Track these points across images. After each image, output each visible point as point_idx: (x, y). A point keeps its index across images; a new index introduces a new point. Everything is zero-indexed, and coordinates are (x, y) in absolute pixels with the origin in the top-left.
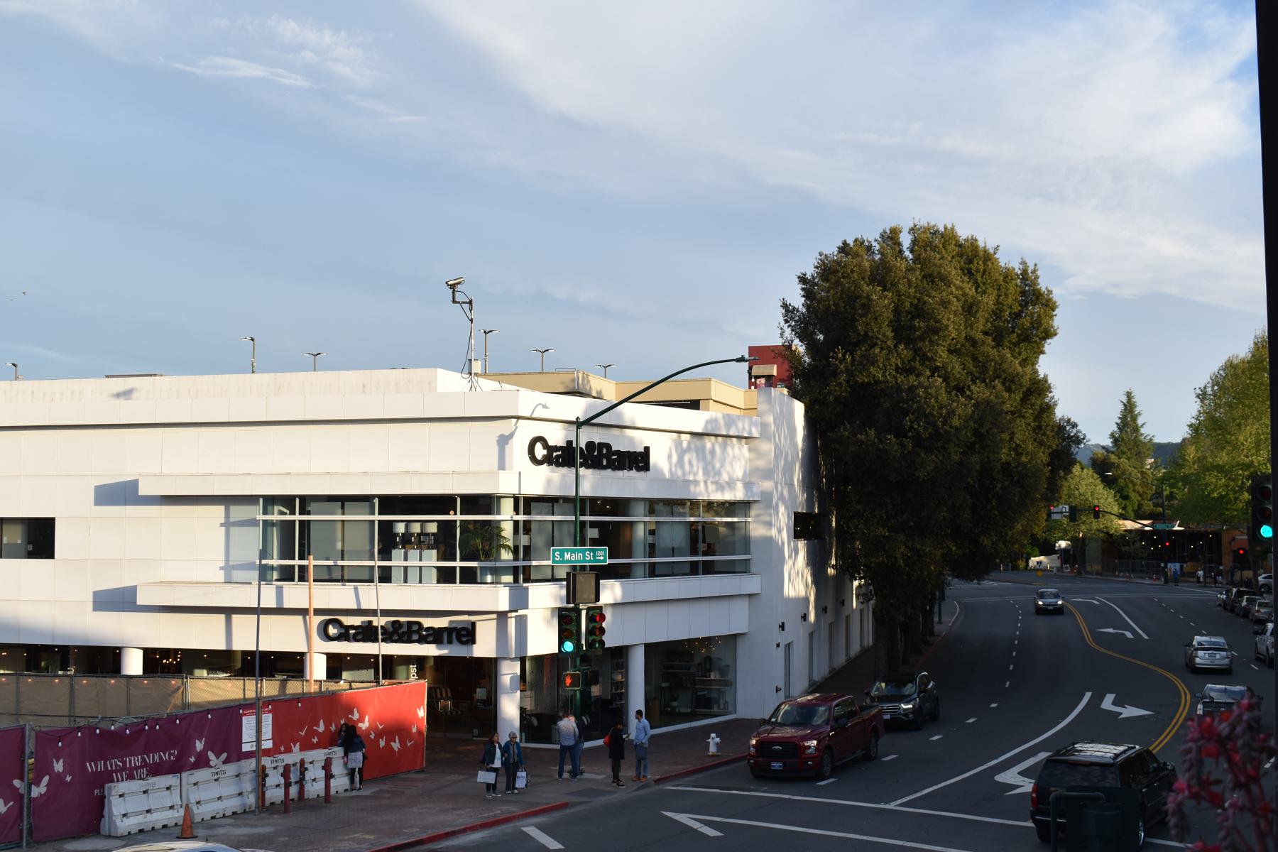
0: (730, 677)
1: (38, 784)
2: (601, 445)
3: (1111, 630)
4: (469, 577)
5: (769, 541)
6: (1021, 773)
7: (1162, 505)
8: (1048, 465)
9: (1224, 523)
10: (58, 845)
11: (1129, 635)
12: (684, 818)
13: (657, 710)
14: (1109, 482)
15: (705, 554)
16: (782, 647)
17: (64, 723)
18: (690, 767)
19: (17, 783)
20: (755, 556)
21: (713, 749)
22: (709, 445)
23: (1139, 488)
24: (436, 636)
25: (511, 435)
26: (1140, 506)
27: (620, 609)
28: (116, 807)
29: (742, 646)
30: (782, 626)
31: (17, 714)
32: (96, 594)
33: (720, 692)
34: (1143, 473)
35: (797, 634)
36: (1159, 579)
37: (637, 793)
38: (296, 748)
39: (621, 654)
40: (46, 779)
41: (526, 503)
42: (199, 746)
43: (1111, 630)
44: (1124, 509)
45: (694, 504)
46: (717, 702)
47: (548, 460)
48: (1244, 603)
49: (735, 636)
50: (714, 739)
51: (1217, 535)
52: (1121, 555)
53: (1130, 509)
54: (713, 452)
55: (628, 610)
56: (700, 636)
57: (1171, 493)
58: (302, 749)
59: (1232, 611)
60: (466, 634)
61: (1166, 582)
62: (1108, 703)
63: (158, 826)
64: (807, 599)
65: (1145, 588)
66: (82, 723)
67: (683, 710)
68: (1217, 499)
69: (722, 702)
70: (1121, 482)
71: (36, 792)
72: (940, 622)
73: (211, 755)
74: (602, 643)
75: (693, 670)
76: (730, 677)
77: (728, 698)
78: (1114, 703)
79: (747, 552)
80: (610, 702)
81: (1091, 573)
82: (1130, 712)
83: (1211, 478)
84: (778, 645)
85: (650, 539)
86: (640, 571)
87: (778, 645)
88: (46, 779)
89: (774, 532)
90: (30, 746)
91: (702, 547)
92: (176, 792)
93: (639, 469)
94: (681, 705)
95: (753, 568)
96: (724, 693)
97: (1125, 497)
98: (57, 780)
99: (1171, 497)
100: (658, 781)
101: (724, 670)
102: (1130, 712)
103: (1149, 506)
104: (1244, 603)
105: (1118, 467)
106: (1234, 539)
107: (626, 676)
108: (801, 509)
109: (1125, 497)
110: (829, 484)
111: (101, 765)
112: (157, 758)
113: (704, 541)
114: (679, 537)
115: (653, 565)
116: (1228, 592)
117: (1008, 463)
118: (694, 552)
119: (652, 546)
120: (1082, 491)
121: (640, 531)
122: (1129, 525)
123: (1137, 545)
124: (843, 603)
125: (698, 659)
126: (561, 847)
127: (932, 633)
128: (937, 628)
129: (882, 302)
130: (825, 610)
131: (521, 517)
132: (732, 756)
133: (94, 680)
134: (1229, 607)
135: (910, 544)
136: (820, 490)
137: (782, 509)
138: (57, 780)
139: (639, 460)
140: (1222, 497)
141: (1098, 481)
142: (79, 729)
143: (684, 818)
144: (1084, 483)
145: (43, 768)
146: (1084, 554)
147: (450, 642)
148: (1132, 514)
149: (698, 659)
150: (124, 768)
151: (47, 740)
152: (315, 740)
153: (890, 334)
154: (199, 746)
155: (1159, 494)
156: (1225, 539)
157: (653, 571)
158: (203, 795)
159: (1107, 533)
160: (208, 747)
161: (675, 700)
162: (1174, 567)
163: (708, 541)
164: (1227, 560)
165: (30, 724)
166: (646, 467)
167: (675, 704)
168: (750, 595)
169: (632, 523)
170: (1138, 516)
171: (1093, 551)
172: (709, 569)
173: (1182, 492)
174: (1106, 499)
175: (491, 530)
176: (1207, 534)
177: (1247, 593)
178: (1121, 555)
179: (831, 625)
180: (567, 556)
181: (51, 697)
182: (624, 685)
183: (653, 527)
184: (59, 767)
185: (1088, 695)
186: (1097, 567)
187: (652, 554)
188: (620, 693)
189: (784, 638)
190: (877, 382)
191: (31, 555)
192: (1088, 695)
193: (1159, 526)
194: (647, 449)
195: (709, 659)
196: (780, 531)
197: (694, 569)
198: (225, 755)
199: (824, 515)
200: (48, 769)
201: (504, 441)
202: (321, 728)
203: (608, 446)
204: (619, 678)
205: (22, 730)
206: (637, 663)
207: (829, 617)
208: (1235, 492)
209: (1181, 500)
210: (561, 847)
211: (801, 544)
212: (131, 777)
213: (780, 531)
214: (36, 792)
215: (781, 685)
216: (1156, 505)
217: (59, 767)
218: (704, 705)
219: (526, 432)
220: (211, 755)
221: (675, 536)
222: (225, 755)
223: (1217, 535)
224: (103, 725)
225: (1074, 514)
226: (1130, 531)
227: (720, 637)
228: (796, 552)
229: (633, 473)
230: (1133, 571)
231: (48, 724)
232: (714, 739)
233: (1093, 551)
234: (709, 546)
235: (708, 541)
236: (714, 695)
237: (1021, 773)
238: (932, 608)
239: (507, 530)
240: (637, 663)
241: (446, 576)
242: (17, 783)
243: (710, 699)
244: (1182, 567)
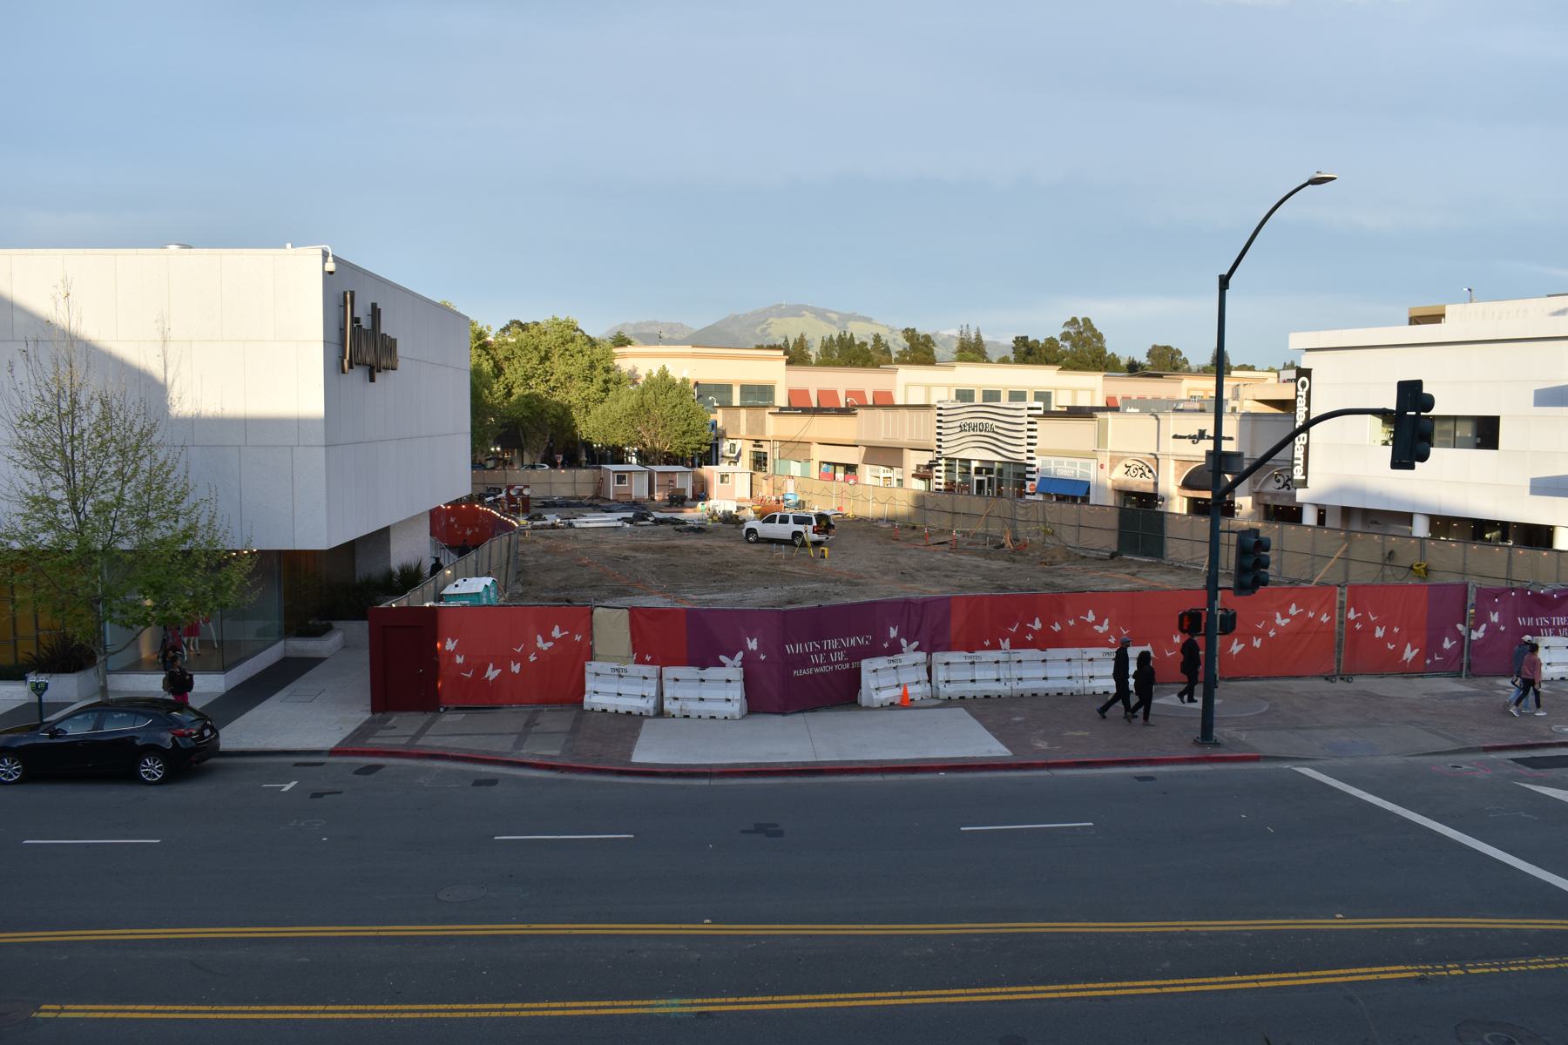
1: (1477, 630)
10: (1491, 680)
17: (1503, 584)
19: (1460, 626)
28: (868, 681)
31: (1463, 573)
32: (1533, 480)
38: (1006, 644)
40: (1484, 627)
42: (893, 633)
58: (1013, 646)
63: (1557, 677)
66: (1516, 585)
71: (1475, 635)
73: (903, 642)
88: (1484, 627)
90: (1472, 599)
92: (667, 693)
98: (1492, 628)
111: (799, 647)
112: (853, 642)
133: (1529, 551)
138: (1492, 628)
142: (1513, 590)
145: (1481, 618)
150: (1550, 626)
151: (1486, 595)
152: (1030, 638)
154: (893, 633)
158: (882, 682)
160: (900, 635)
165: (1473, 582)
181: (1491, 565)
184: (1495, 618)
185: (48, 1011)
191: (1479, 446)
198: (916, 644)
200: (1486, 619)
202: (1038, 625)
205: (1466, 586)
212: (1556, 634)
214: (1475, 635)
217: (1495, 618)
220: (903, 642)
222: (916, 644)
224: (1534, 588)
231: (1488, 583)
242: (1460, 626)
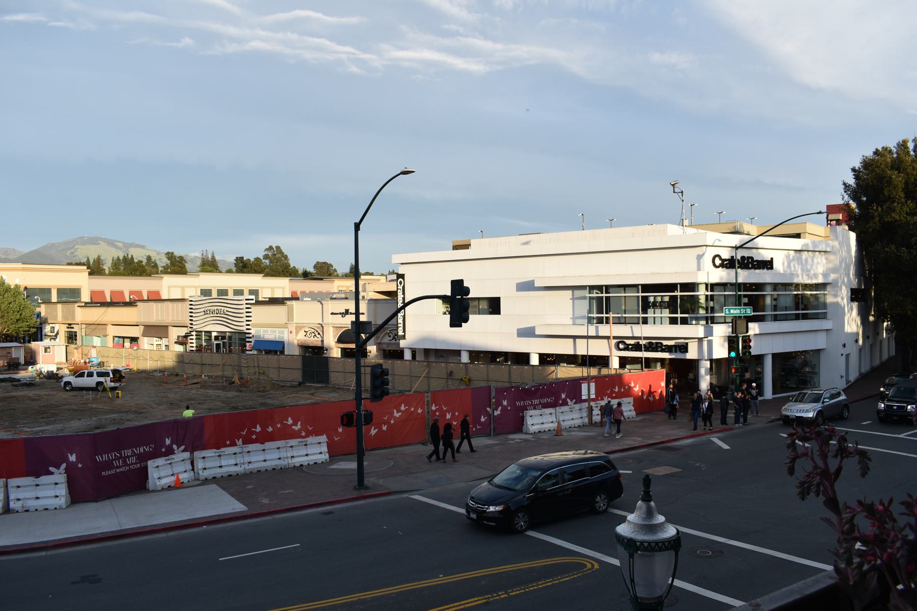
0: (816, 370)
2: (748, 258)
4: (684, 321)
5: (837, 304)
22: (804, 257)
24: (669, 349)
25: (703, 254)
29: (823, 356)
30: (844, 345)
39: (760, 358)
41: (712, 287)
47: (722, 265)
49: (819, 350)
54: (806, 260)
60: (684, 348)
64: (858, 334)
74: (750, 353)
76: (816, 370)
77: (815, 380)
85: (774, 303)
86: (769, 318)
91: (801, 306)
93: (768, 269)
95: (829, 316)
110: (870, 273)
114: (789, 302)
118: (797, 309)
121: (768, 301)
129: (898, 179)
130: (868, 337)
131: (709, 293)
136: (865, 277)
137: (844, 288)
139: (768, 265)
147: (676, 352)
153: (902, 195)
157: (776, 318)
163: (804, 303)
166: (772, 268)
168: (827, 330)
172: (805, 317)
175: (695, 299)
179: (871, 345)
180: (732, 311)
187: (775, 310)
189: (845, 351)
190: (896, 221)
194: (772, 259)
196: (842, 299)
197: (797, 317)
199: (867, 290)
201: (700, 257)
203: (752, 258)
211: (855, 305)
215: (844, 374)
219: (710, 253)
229: (765, 270)
239: (702, 300)
241: (673, 321)
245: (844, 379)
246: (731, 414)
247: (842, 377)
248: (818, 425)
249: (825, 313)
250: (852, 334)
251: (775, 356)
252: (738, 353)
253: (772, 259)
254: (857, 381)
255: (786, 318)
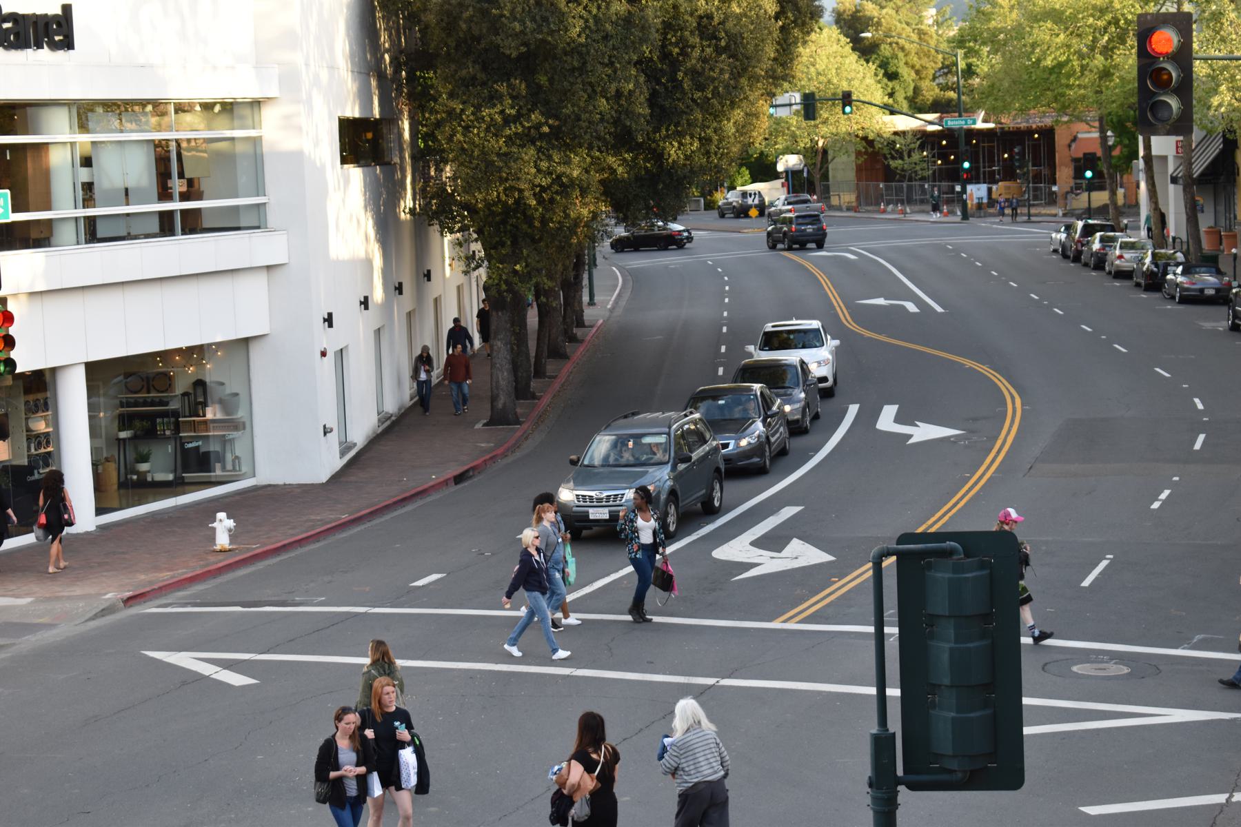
0: (241, 414)
3: (881, 301)
5: (297, 157)
6: (755, 544)
7: (955, 88)
8: (777, 17)
9: (1063, 109)
11: (911, 307)
12: (185, 660)
13: (118, 484)
14: (865, 50)
15: (184, 197)
16: (330, 354)
18: (182, 573)
20: (274, 197)
21: (223, 540)
23: (914, 59)
26: (916, 90)
27: (37, 301)
29: (257, 354)
30: (329, 320)
33: (224, 441)
34: (921, 33)
35: (355, 331)
36: (951, 212)
37: (93, 624)
39: (40, 386)
43: (881, 301)
44: (891, 95)
45: (158, 106)
46: (221, 459)
48: (1096, 246)
49: (246, 341)
50: (223, 525)
51: (1048, 134)
52: (889, 175)
53: (900, 96)
55: (52, 303)
56: (183, 343)
57: (969, 66)
59: (1077, 258)
61: (965, 216)
62: (887, 420)
64: (369, 262)
65: (928, 229)
67: (160, 477)
68: (1051, 70)
69: (229, 457)
70: (885, 50)
72: (592, 303)
74: (11, 364)
75: (174, 405)
76: (241, 414)
77: (240, 449)
78: (898, 419)
79: (259, 189)
80: (29, 469)
81: (839, 208)
82: (924, 432)
83: (1043, 32)
84: (323, 354)
85: (84, 175)
86: (67, 233)
87: (323, 354)
89: (308, 148)
91: (178, 186)
93: (55, 46)
94: (158, 468)
95: (272, 218)
96: (232, 441)
97: (892, 76)
99: (969, 72)
100: (129, 601)
101: (229, 404)
102: (924, 432)
103: (931, 91)
104: (1096, 246)
105: (879, 24)
106: (1075, 139)
107: (56, 422)
108: (353, 111)
109: (892, 76)
110: (397, 71)
113: (181, 175)
114: (136, 170)
115: (91, 222)
116: (1069, 228)
117: (710, 17)
118: (165, 195)
119: (88, 187)
120: (821, 66)
121: (59, 160)
122: (905, 123)
123: (916, 157)
124: (428, 276)
125: (181, 386)
126: (832, 558)
127: (580, 323)
128: (589, 313)
130: (399, 289)
132: (257, 548)
134: (1072, 254)
135: (544, 165)
136: (381, 76)
140: (1060, 65)
141: (848, 48)
143: (185, 660)
144: (822, 53)
146: (825, 177)
148: (905, 105)
149: (181, 386)
155: (948, 69)
156: (1061, 139)
157: (92, 232)
159: (865, 138)
161: (145, 459)
162: (977, 192)
164: (1064, 174)
167: (144, 467)
169: (45, 145)
170: (917, 107)
171: (843, 168)
172: (192, 224)
173: (987, 63)
174: (862, 78)
176: (1030, 132)
177: (1102, 228)
178: (889, 175)
179: (409, 315)
182: (50, 439)
183: (88, 150)
186: (849, 198)
187: (88, 201)
188: (45, 449)
189: (331, 340)
192: (853, 409)
193: (954, 122)
194: (67, 9)
195: (200, 384)
197: (166, 225)
199: (389, 120)
204: (40, 426)
206: (73, 399)
207: (407, 301)
208: (1081, 56)
209: (987, 76)
210: (832, 558)
211: (356, 174)
213: (316, 144)
215: (332, 423)
216: (944, 88)
218: (196, 464)
221: (127, 167)
223: (1048, 134)
225: (810, 106)
226: (903, 134)
227: (220, 345)
228: (347, 181)
229: (45, 53)
230: (910, 201)
232: (223, 525)
233: (843, 168)
234: (190, 182)
235: (187, 175)
236: (214, 447)
237: (755, 544)
238: (578, 278)
240: (73, 399)
243: (207, 454)
244: (990, 190)
245: (334, 437)
246: (941, 80)
247: (326, 431)
248: (460, 125)
249: (259, 207)
250: (353, 262)
251: (96, 371)
252: (869, 416)
253: (67, 9)
254: (375, 441)
255: (125, 230)
